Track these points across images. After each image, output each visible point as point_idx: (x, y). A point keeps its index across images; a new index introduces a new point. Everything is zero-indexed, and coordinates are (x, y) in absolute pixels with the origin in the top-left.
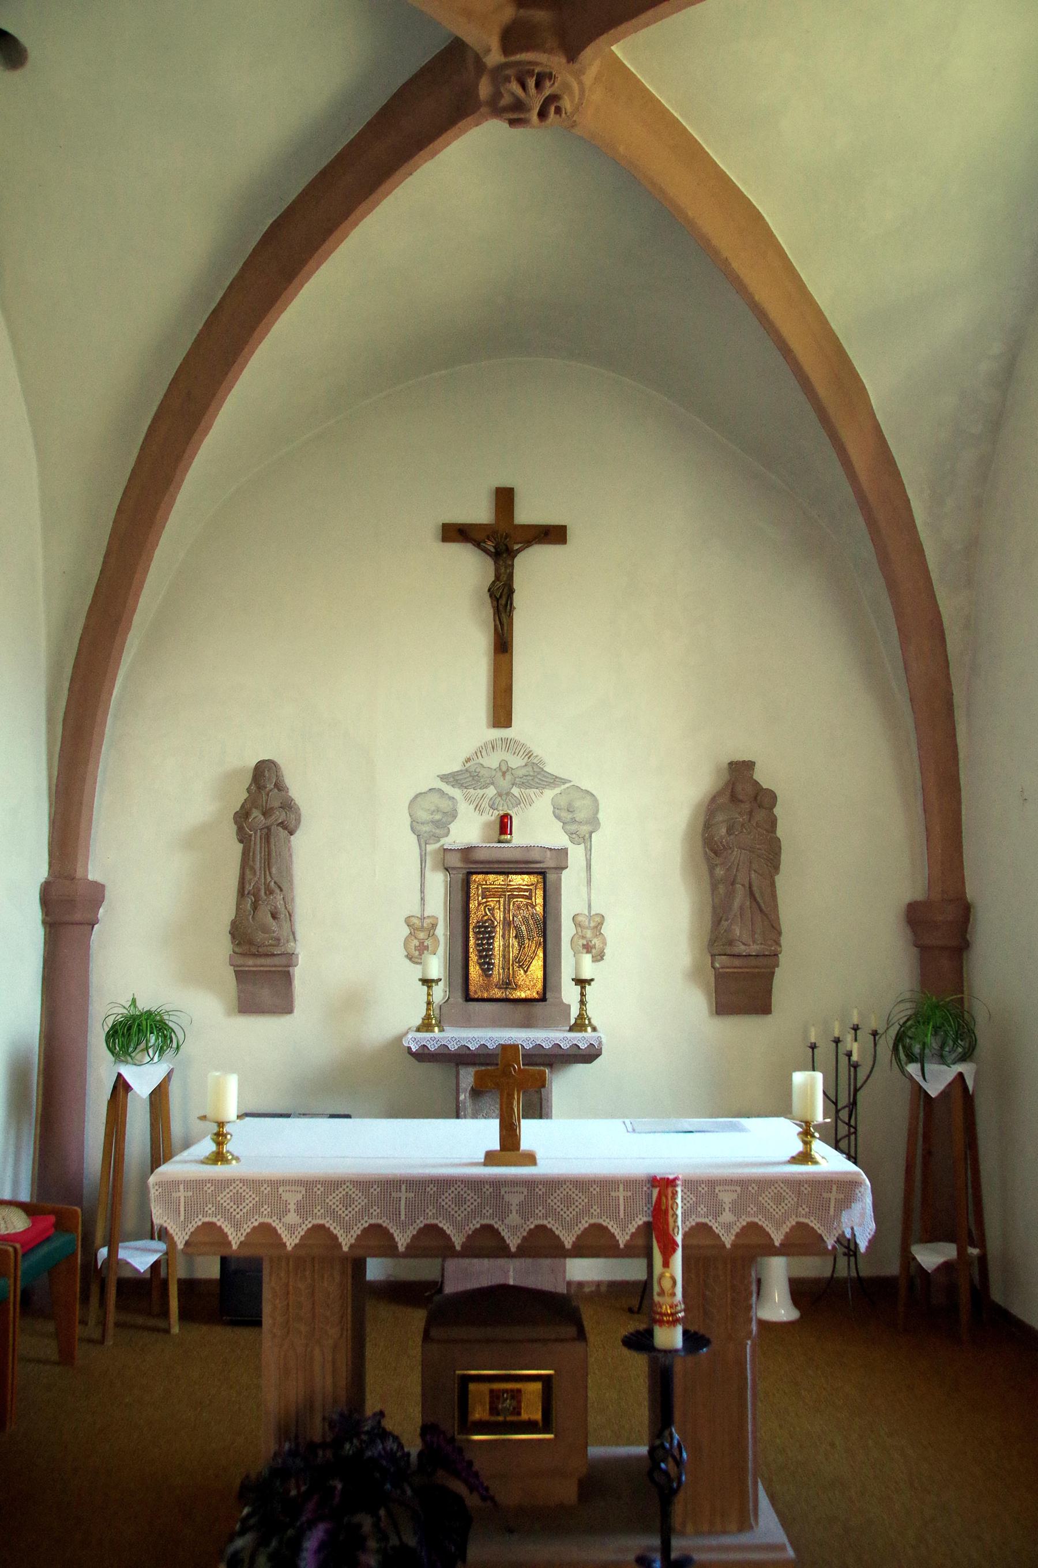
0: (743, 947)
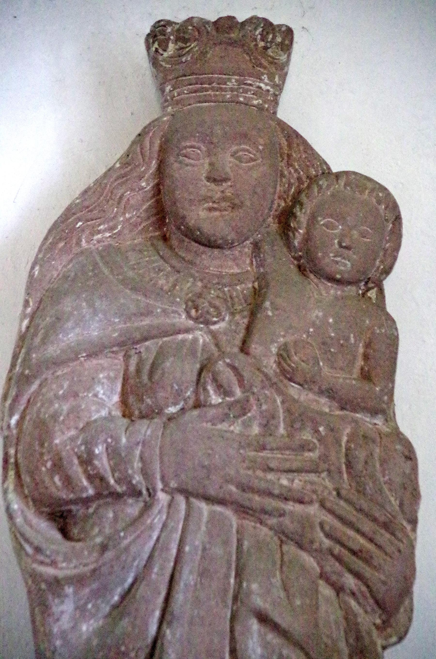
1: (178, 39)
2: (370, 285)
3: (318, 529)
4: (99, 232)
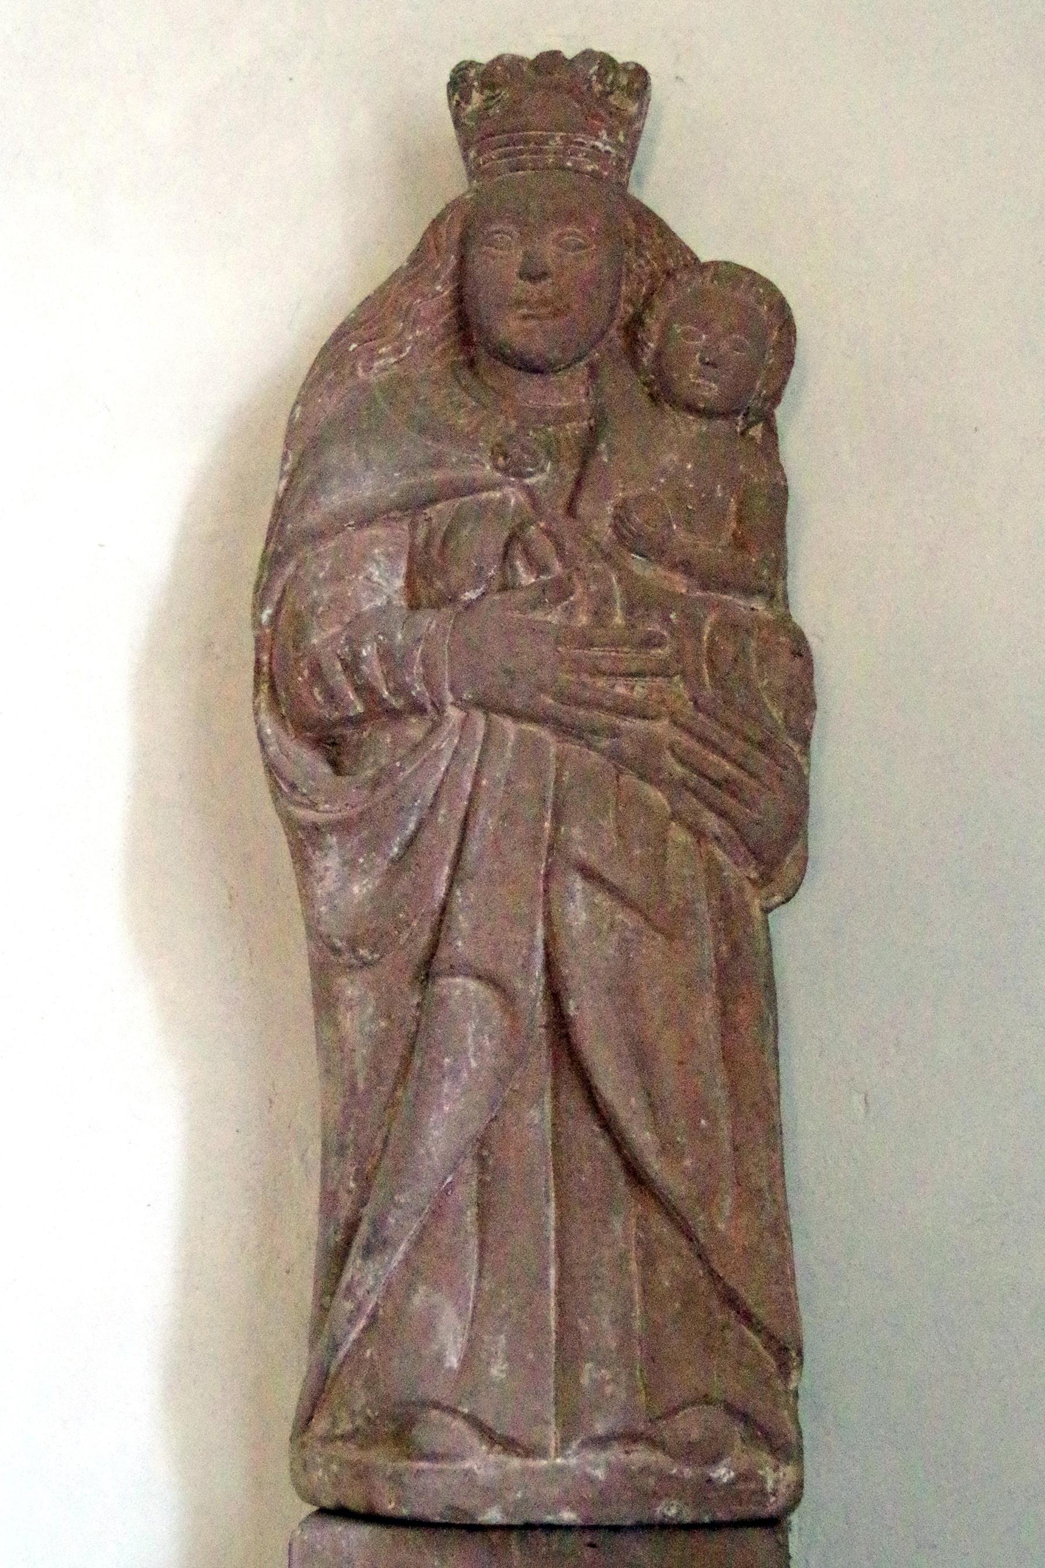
0: (482, 1462)
1: (483, 86)
2: (751, 418)
3: (668, 753)
4: (381, 356)
